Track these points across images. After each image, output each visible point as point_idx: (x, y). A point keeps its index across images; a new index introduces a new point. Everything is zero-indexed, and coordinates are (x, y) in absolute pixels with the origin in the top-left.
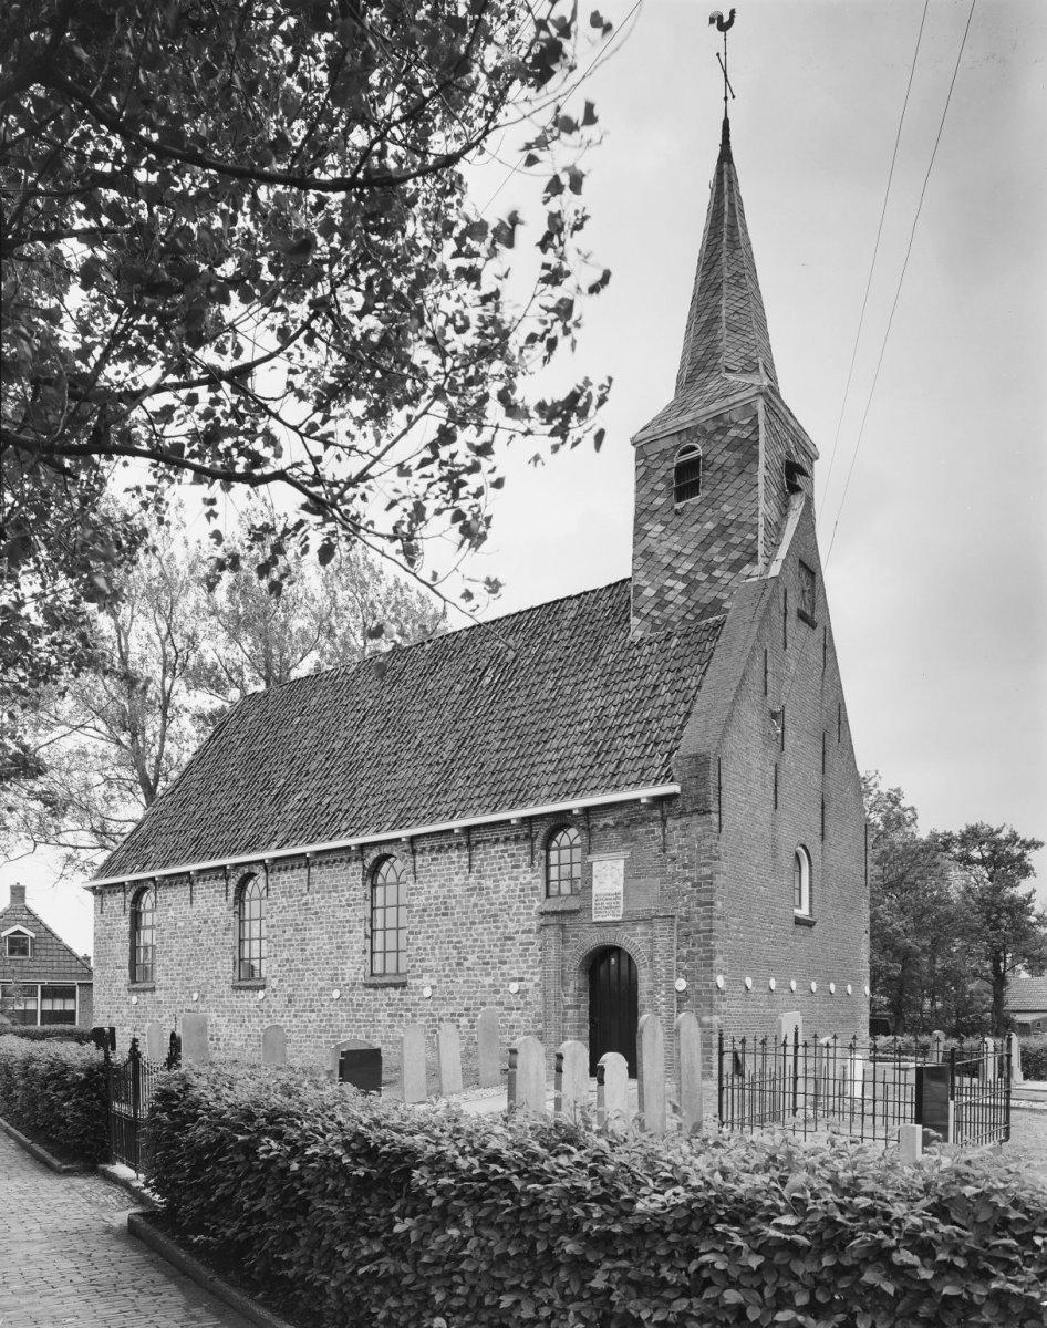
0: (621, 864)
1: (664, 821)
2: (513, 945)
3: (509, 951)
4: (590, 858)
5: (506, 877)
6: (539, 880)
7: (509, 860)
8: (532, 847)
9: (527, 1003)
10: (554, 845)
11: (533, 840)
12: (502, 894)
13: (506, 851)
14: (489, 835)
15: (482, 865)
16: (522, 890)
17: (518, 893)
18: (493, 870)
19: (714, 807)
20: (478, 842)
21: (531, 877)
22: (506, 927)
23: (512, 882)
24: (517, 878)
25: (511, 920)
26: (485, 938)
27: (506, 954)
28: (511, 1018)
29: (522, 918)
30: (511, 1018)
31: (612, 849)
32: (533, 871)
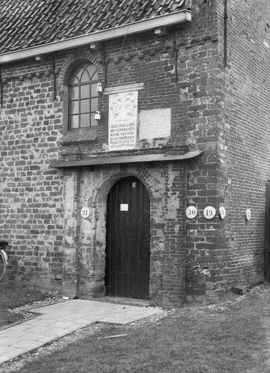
0: (135, 95)
1: (176, 51)
2: (38, 173)
3: (35, 179)
4: (109, 90)
5: (32, 111)
6: (61, 114)
7: (35, 95)
8: (55, 83)
9: (49, 227)
10: (76, 81)
11: (56, 75)
12: (28, 127)
13: (30, 88)
14: (18, 73)
15: (11, 101)
16: (46, 123)
17: (42, 126)
18: (21, 105)
19: (220, 38)
20: (9, 80)
21: (52, 110)
22: (32, 157)
23: (38, 116)
24: (41, 113)
25: (37, 151)
26: (15, 167)
27: (32, 182)
28: (36, 240)
29: (46, 149)
30: (36, 240)
31: (127, 81)
32: (56, 105)
